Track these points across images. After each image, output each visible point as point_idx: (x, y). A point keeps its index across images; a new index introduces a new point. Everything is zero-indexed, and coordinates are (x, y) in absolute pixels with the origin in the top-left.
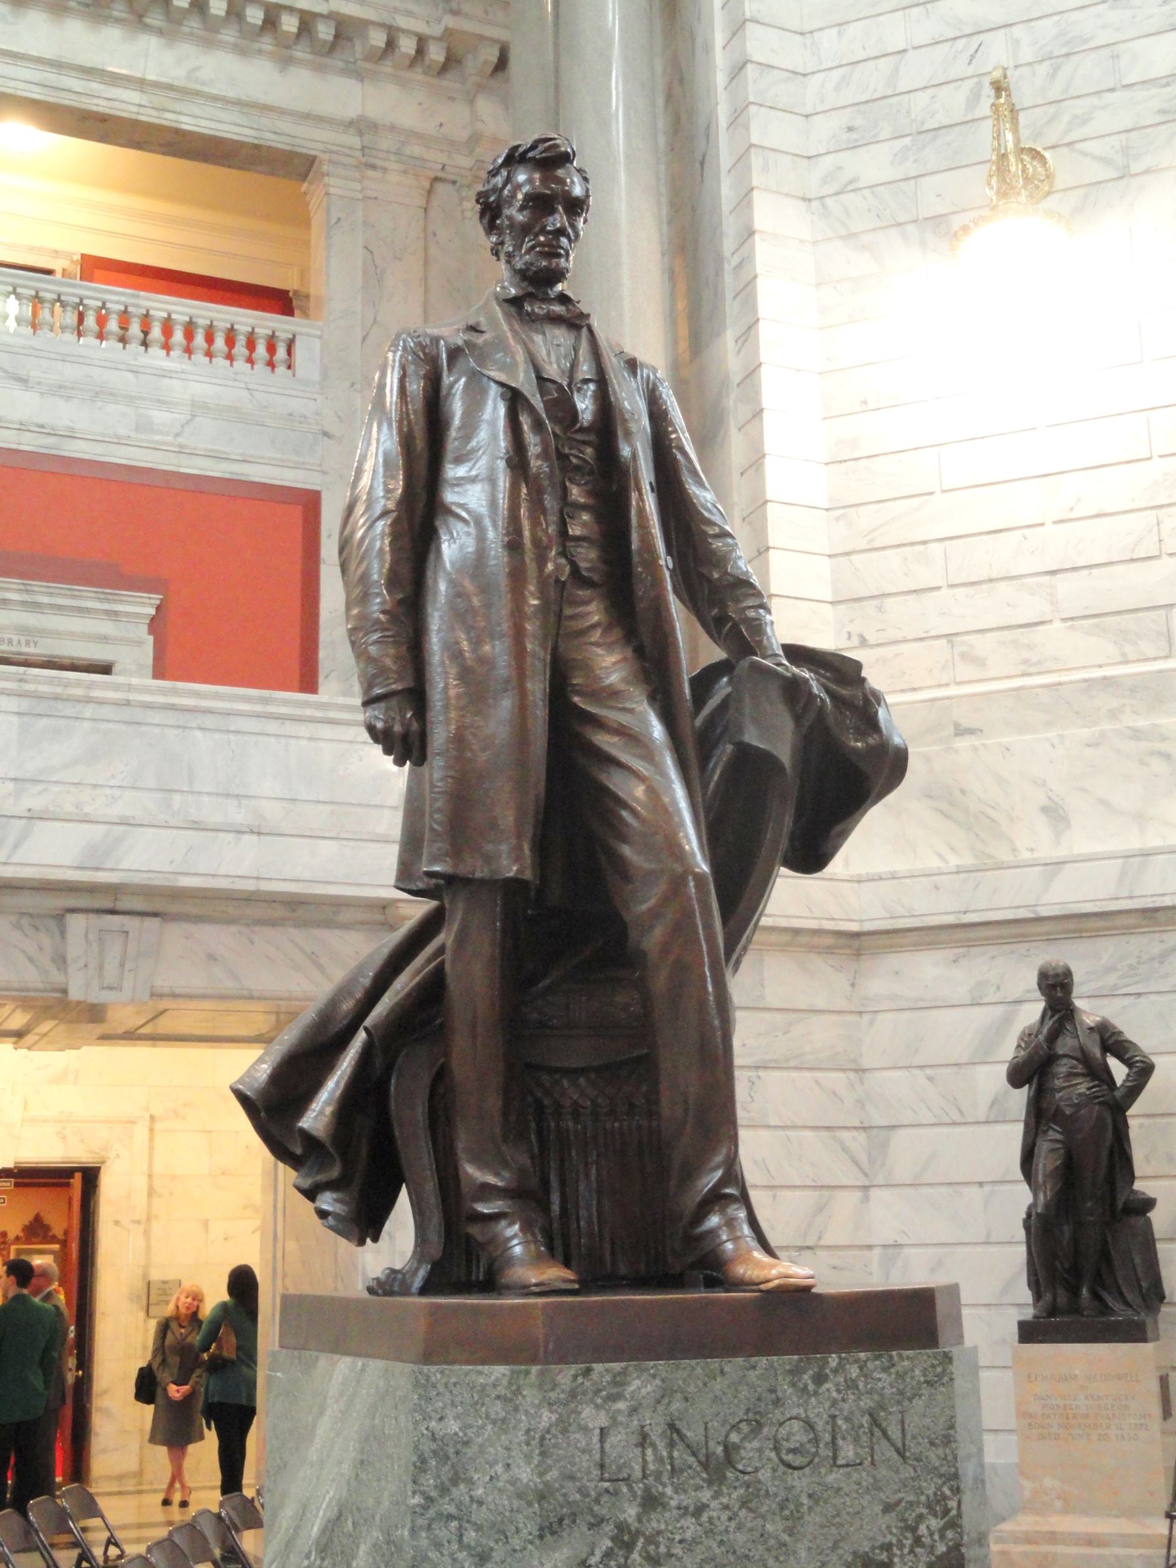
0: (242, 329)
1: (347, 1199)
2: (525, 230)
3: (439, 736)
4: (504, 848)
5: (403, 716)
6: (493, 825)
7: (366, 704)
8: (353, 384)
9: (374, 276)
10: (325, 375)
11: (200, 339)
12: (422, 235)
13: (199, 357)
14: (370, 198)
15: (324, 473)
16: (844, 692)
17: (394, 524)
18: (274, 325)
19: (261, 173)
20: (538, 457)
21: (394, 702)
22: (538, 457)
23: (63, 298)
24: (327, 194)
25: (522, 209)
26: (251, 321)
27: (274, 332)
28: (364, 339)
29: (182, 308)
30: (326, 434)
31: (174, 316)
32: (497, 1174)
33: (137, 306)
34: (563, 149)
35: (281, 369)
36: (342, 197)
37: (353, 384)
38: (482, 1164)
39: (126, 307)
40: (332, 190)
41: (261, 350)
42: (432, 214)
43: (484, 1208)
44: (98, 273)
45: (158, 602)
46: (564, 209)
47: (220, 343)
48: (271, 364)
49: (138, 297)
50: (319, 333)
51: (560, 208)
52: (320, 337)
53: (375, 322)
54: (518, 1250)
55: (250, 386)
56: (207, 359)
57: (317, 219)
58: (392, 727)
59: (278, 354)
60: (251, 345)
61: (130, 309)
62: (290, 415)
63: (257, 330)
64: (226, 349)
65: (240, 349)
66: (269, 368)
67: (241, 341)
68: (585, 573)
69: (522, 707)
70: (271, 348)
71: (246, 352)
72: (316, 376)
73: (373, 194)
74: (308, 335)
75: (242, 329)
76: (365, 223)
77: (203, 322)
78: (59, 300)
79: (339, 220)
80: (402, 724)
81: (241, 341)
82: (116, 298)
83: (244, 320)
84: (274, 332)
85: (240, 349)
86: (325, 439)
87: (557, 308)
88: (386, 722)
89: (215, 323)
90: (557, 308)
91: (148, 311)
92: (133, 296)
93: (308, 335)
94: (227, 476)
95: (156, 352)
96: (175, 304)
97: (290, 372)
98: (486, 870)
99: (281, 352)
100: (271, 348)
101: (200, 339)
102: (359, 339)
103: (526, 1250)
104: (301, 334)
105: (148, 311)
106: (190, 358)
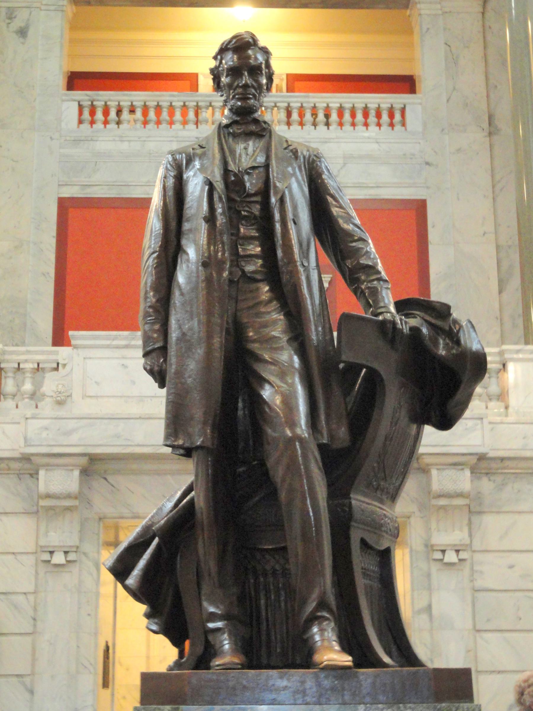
0: (373, 106)
1: (159, 622)
2: (230, 86)
3: (172, 369)
4: (197, 430)
5: (158, 362)
6: (192, 418)
7: (146, 355)
8: (443, 130)
9: (452, 61)
10: (425, 125)
11: (347, 116)
12: (482, 30)
13: (347, 127)
14: (446, 12)
15: (428, 188)
16: (439, 323)
17: (158, 257)
18: (392, 101)
19: (382, 8)
20: (221, 214)
21: (154, 355)
22: (221, 214)
23: (278, 105)
24: (420, 15)
25: (227, 77)
26: (378, 101)
27: (392, 105)
28: (448, 101)
29: (335, 100)
30: (427, 163)
31: (330, 105)
32: (218, 607)
33: (308, 102)
34: (247, 39)
35: (398, 127)
36: (429, 15)
37: (443, 130)
38: (213, 603)
39: (302, 104)
40: (422, 12)
41: (385, 117)
42: (487, 15)
43: (211, 625)
44: (298, 84)
45: (329, 279)
46: (248, 73)
47: (359, 117)
48: (392, 125)
49: (308, 97)
50: (419, 101)
51: (246, 73)
52: (421, 104)
53: (454, 89)
54: (227, 647)
55: (378, 141)
56: (352, 128)
57: (416, 30)
58: (154, 368)
59: (395, 118)
60: (379, 115)
61: (304, 105)
62: (404, 155)
63: (381, 105)
64: (363, 120)
65: (372, 119)
66: (391, 128)
67: (372, 113)
68: (249, 275)
69: (209, 353)
70: (391, 115)
71: (375, 120)
72: (420, 129)
73: (448, 10)
74: (413, 103)
75: (373, 106)
76: (445, 29)
77: (348, 106)
78: (276, 106)
79: (428, 29)
80: (158, 366)
81: (372, 113)
82: (295, 99)
83: (372, 100)
84: (392, 105)
85: (372, 119)
86: (427, 166)
87: (253, 128)
88: (150, 366)
89: (355, 105)
90: (253, 128)
91: (315, 105)
92: (305, 97)
93: (413, 103)
94: (367, 197)
95: (321, 128)
96: (331, 98)
97: (403, 128)
98: (189, 442)
99: (398, 117)
100: (391, 115)
101: (347, 116)
102: (445, 100)
103: (231, 648)
104: (409, 104)
105: (315, 105)
106: (341, 129)
